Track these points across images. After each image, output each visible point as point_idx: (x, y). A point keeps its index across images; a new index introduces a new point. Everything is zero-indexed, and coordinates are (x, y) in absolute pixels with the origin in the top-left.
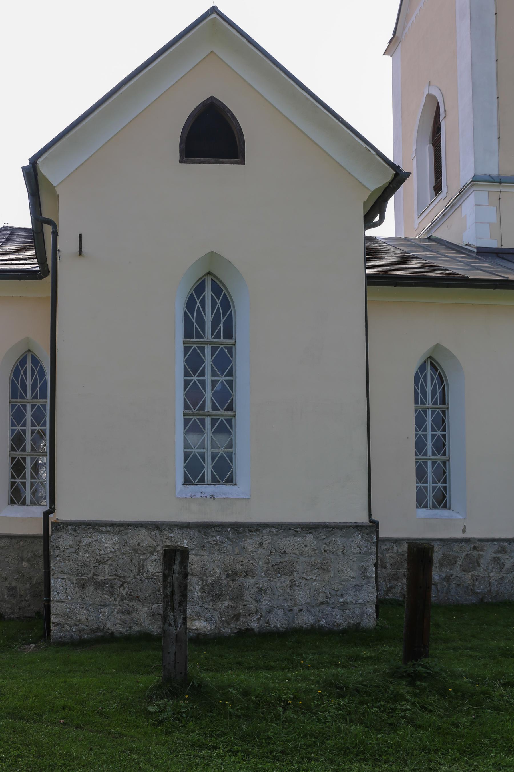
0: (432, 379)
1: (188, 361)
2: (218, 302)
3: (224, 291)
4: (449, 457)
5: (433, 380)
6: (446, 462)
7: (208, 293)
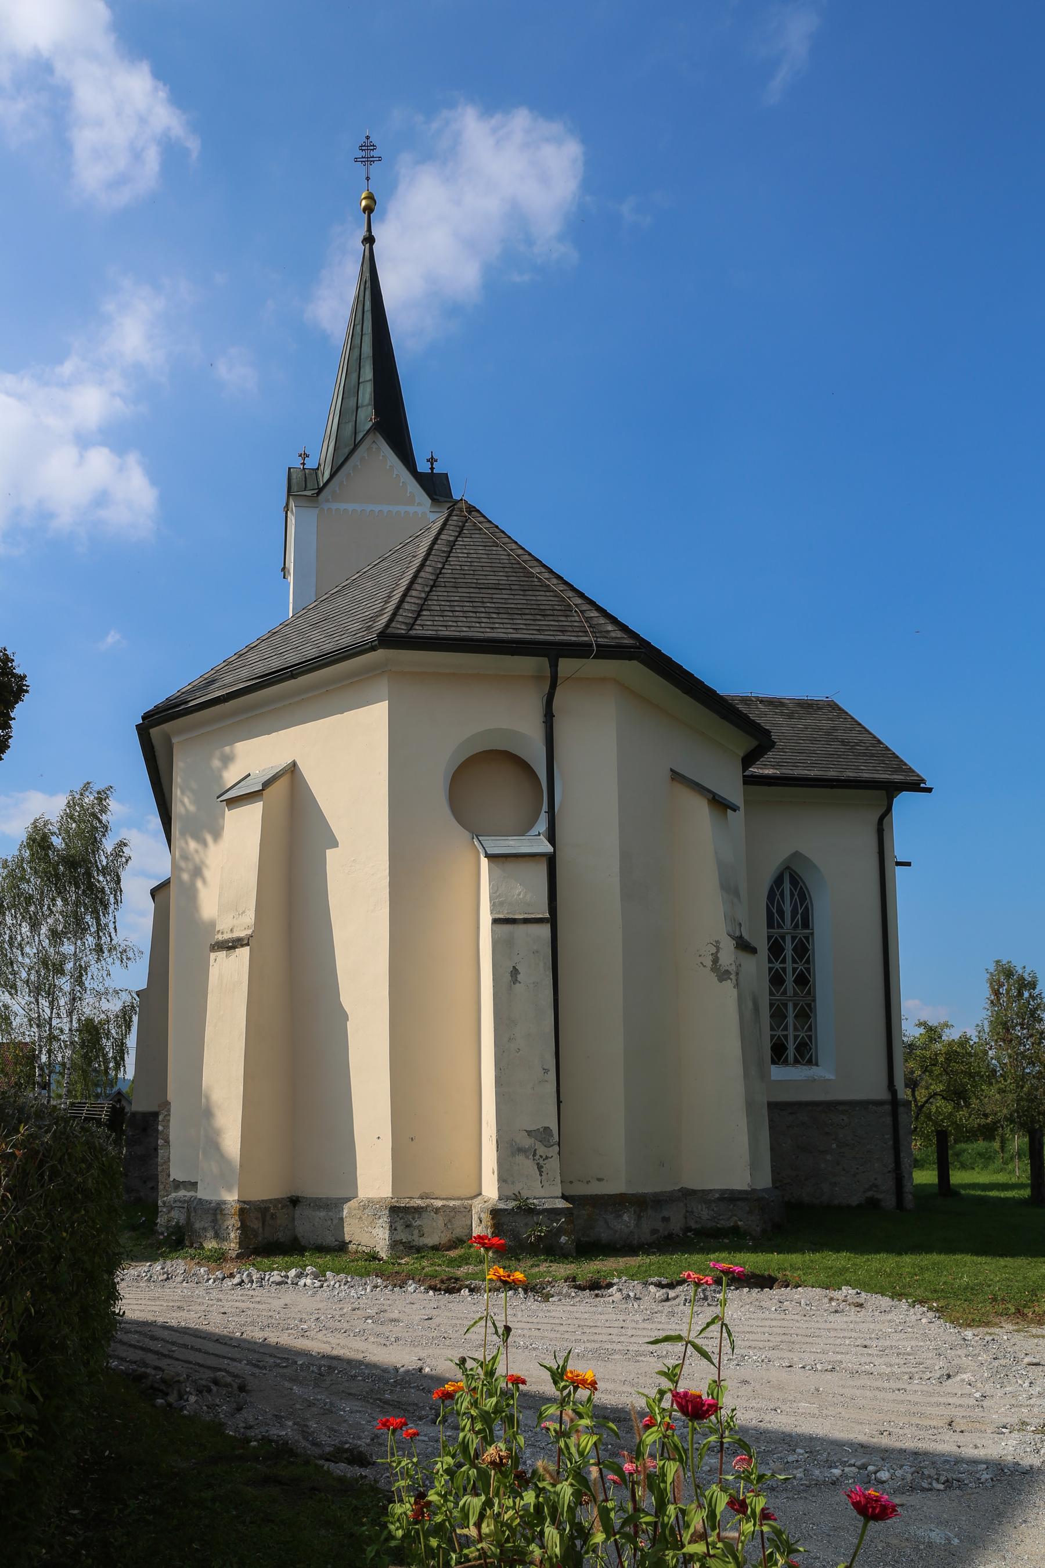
0: (792, 895)
4: (814, 997)
7: (787, 886)
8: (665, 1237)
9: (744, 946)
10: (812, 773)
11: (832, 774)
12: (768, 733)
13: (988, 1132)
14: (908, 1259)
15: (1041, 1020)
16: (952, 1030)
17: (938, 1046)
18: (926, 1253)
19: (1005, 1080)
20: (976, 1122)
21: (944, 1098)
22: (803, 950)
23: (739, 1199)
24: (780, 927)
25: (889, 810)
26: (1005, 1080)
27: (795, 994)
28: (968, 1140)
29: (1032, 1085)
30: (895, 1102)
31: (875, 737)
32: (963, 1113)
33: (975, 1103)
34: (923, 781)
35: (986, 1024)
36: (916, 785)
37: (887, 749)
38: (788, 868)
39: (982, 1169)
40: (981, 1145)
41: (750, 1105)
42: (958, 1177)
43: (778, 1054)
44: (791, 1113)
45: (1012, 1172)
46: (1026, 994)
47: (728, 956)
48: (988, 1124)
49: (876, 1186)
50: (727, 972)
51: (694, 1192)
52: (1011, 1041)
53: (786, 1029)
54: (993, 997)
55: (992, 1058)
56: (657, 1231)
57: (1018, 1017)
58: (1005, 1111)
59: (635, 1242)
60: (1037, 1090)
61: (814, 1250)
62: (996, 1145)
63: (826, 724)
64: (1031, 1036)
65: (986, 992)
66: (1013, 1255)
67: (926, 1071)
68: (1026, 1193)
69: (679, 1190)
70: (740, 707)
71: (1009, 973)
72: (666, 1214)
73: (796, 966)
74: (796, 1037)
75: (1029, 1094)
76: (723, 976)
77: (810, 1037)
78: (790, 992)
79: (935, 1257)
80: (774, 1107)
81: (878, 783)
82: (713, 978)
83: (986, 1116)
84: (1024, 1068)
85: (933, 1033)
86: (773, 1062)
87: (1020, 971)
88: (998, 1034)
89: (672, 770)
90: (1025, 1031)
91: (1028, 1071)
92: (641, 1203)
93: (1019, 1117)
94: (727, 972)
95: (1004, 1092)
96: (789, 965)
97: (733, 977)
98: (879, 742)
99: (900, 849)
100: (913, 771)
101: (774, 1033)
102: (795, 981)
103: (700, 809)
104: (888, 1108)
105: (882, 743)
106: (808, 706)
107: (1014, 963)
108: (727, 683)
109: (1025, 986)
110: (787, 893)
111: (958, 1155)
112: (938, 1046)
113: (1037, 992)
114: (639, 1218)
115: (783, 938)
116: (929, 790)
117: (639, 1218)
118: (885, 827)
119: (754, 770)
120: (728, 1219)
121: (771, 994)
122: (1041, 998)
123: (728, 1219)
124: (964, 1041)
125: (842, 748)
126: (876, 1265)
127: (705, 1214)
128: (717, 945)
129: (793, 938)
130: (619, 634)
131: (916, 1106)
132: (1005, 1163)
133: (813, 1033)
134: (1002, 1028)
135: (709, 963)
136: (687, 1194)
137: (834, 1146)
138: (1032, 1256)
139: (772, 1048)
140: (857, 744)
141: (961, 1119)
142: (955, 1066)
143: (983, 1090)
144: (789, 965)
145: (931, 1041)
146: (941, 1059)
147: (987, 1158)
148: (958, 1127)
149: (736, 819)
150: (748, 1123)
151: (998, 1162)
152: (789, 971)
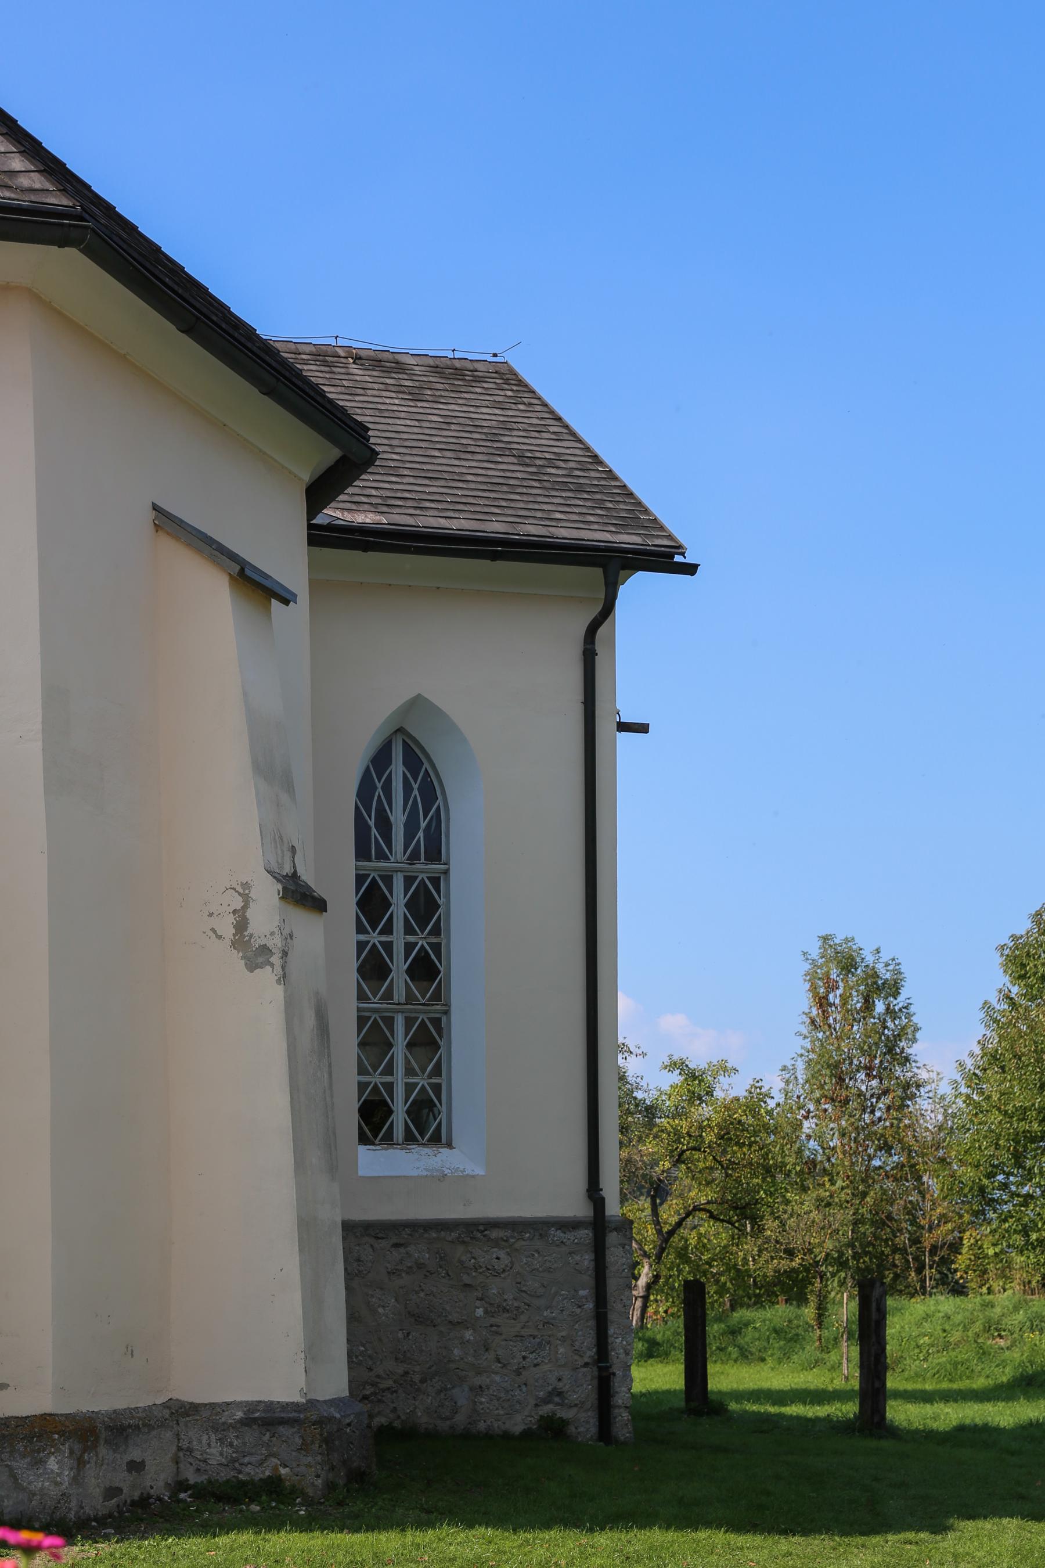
0: (407, 789)
1: (363, 904)
2: (416, 786)
3: (426, 765)
4: (448, 1005)
5: (401, 793)
6: (440, 1019)
7: (398, 769)
8: (134, 1503)
9: (299, 895)
10: (454, 524)
11: (495, 527)
12: (360, 431)
13: (794, 1286)
14: (603, 1539)
15: (907, 1059)
16: (735, 1078)
17: (705, 1111)
18: (642, 1527)
19: (833, 1184)
20: (771, 1266)
21: (712, 1216)
22: (426, 907)
23: (282, 1422)
24: (382, 856)
25: (608, 610)
26: (833, 1182)
27: (410, 997)
28: (758, 1303)
29: (884, 1192)
30: (600, 1226)
31: (587, 449)
32: (750, 1246)
33: (770, 1225)
34: (679, 549)
35: (801, 1065)
36: (666, 559)
37: (611, 475)
38: (401, 730)
39: (780, 1361)
40: (780, 1312)
41: (307, 1227)
42: (725, 1377)
43: (373, 1120)
44: (397, 1245)
45: (835, 1367)
46: (880, 1007)
47: (268, 911)
48: (793, 1270)
49: (560, 1394)
50: (265, 950)
51: (194, 1408)
52: (847, 1101)
53: (389, 1070)
54: (815, 1012)
55: (809, 1137)
56: (118, 1491)
57: (863, 1053)
58: (829, 1245)
59: (72, 1515)
60: (891, 1202)
61: (422, 1525)
62: (809, 1312)
63: (488, 416)
64: (886, 1092)
65: (803, 1002)
66: (806, 1532)
67: (679, 1160)
68: (850, 1409)
69: (165, 1405)
70: (313, 372)
71: (848, 963)
72: (135, 1454)
73: (411, 939)
74: (409, 1088)
75: (875, 1211)
76: (256, 957)
77: (437, 1088)
78: (399, 994)
79: (657, 1536)
80: (355, 1232)
81: (596, 553)
82: (236, 960)
83: (790, 1253)
84: (870, 1158)
85: (696, 1084)
86: (363, 1140)
87: (870, 959)
88: (822, 1087)
89: (155, 507)
90: (874, 1083)
91: (876, 1163)
92: (84, 1433)
93: (856, 1256)
94: (265, 950)
95: (828, 1205)
96: (399, 939)
97: (276, 959)
98: (596, 459)
99: (627, 698)
100: (662, 528)
101: (365, 1079)
102: (410, 971)
103: (213, 591)
104: (586, 1235)
105: (601, 463)
106: (456, 373)
107: (860, 942)
108: (278, 315)
109: (879, 989)
110: (398, 786)
111: (734, 1332)
112: (705, 1111)
113: (900, 1002)
114: (81, 1463)
115: (388, 880)
116: (690, 569)
117: (81, 1463)
118: (598, 648)
119: (334, 513)
120: (261, 1463)
121: (362, 997)
122: (909, 1016)
123: (261, 1463)
124: (757, 1098)
125: (520, 472)
126: (540, 1553)
127: (214, 1454)
128: (245, 892)
129: (409, 881)
130: (37, 181)
131: (659, 1232)
132: (825, 1349)
133: (442, 1080)
134: (831, 1075)
135: (228, 931)
136: (182, 1412)
137: (480, 1312)
138: (844, 1533)
139: (360, 1110)
140: (550, 463)
141: (745, 1259)
142: (736, 1154)
143: (787, 1202)
144: (399, 939)
145: (691, 1102)
146: (709, 1137)
147: (789, 1339)
148: (740, 1275)
149: (292, 620)
150: (302, 1265)
151: (811, 1350)
152: (399, 949)
